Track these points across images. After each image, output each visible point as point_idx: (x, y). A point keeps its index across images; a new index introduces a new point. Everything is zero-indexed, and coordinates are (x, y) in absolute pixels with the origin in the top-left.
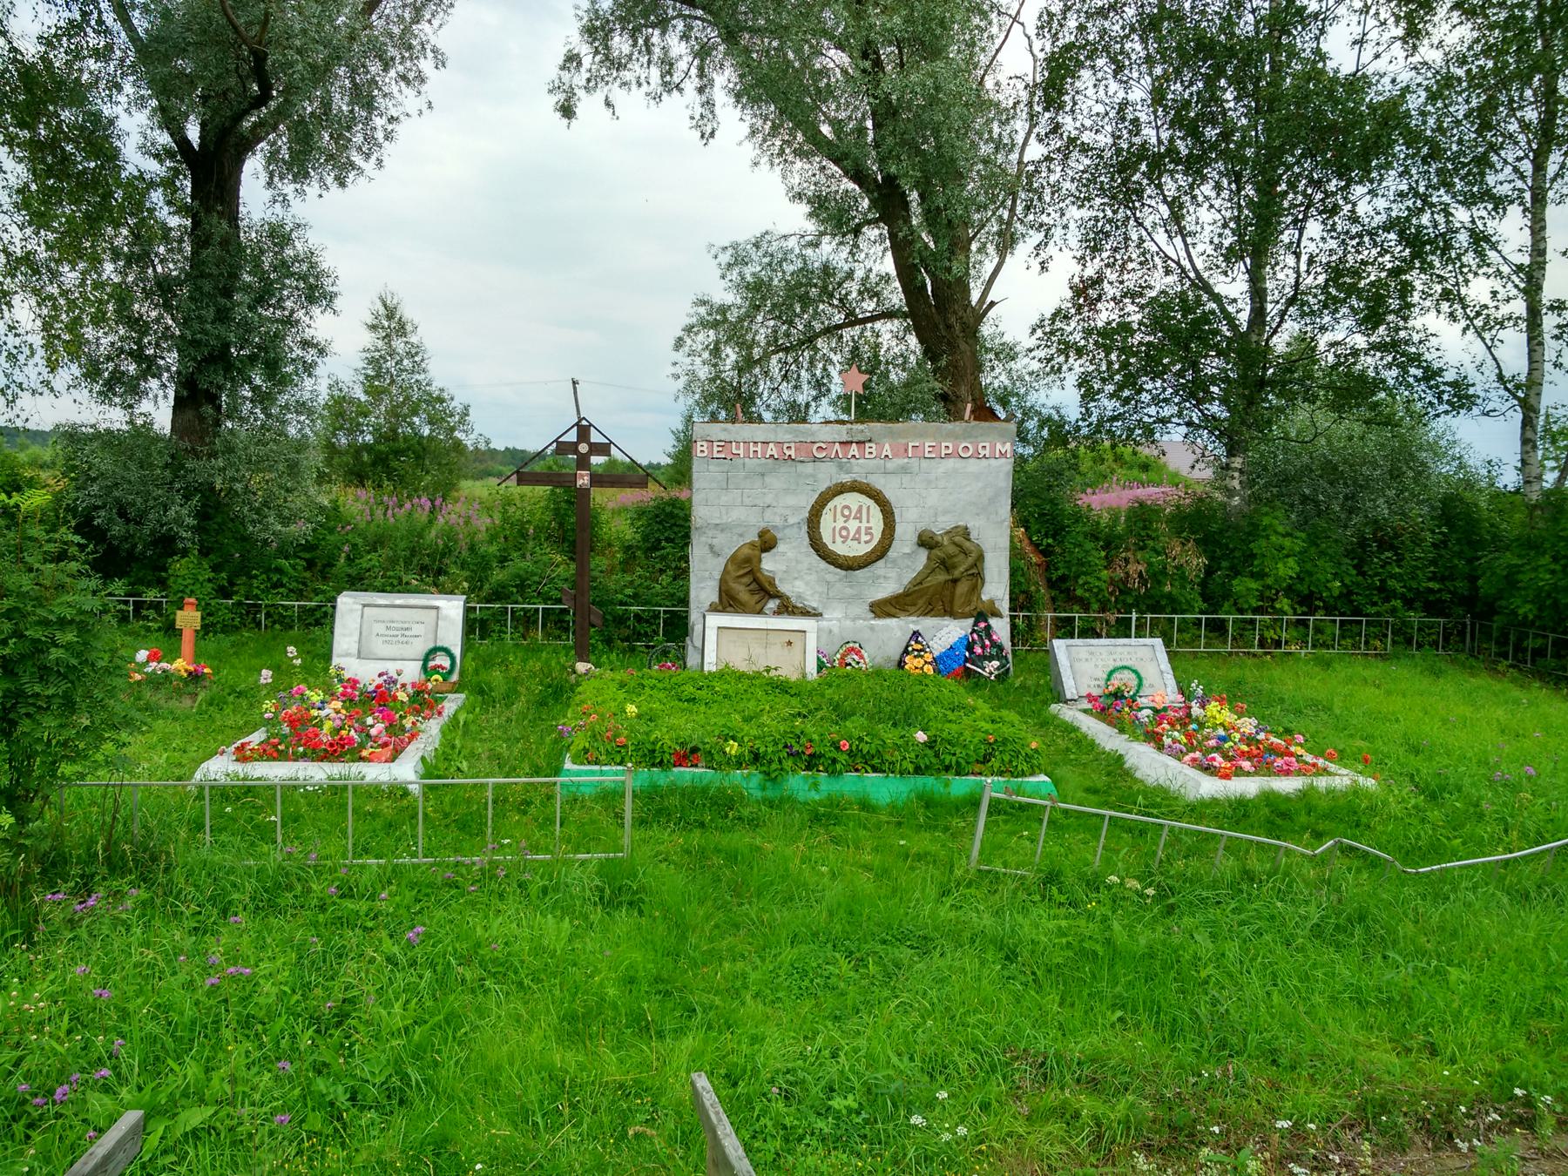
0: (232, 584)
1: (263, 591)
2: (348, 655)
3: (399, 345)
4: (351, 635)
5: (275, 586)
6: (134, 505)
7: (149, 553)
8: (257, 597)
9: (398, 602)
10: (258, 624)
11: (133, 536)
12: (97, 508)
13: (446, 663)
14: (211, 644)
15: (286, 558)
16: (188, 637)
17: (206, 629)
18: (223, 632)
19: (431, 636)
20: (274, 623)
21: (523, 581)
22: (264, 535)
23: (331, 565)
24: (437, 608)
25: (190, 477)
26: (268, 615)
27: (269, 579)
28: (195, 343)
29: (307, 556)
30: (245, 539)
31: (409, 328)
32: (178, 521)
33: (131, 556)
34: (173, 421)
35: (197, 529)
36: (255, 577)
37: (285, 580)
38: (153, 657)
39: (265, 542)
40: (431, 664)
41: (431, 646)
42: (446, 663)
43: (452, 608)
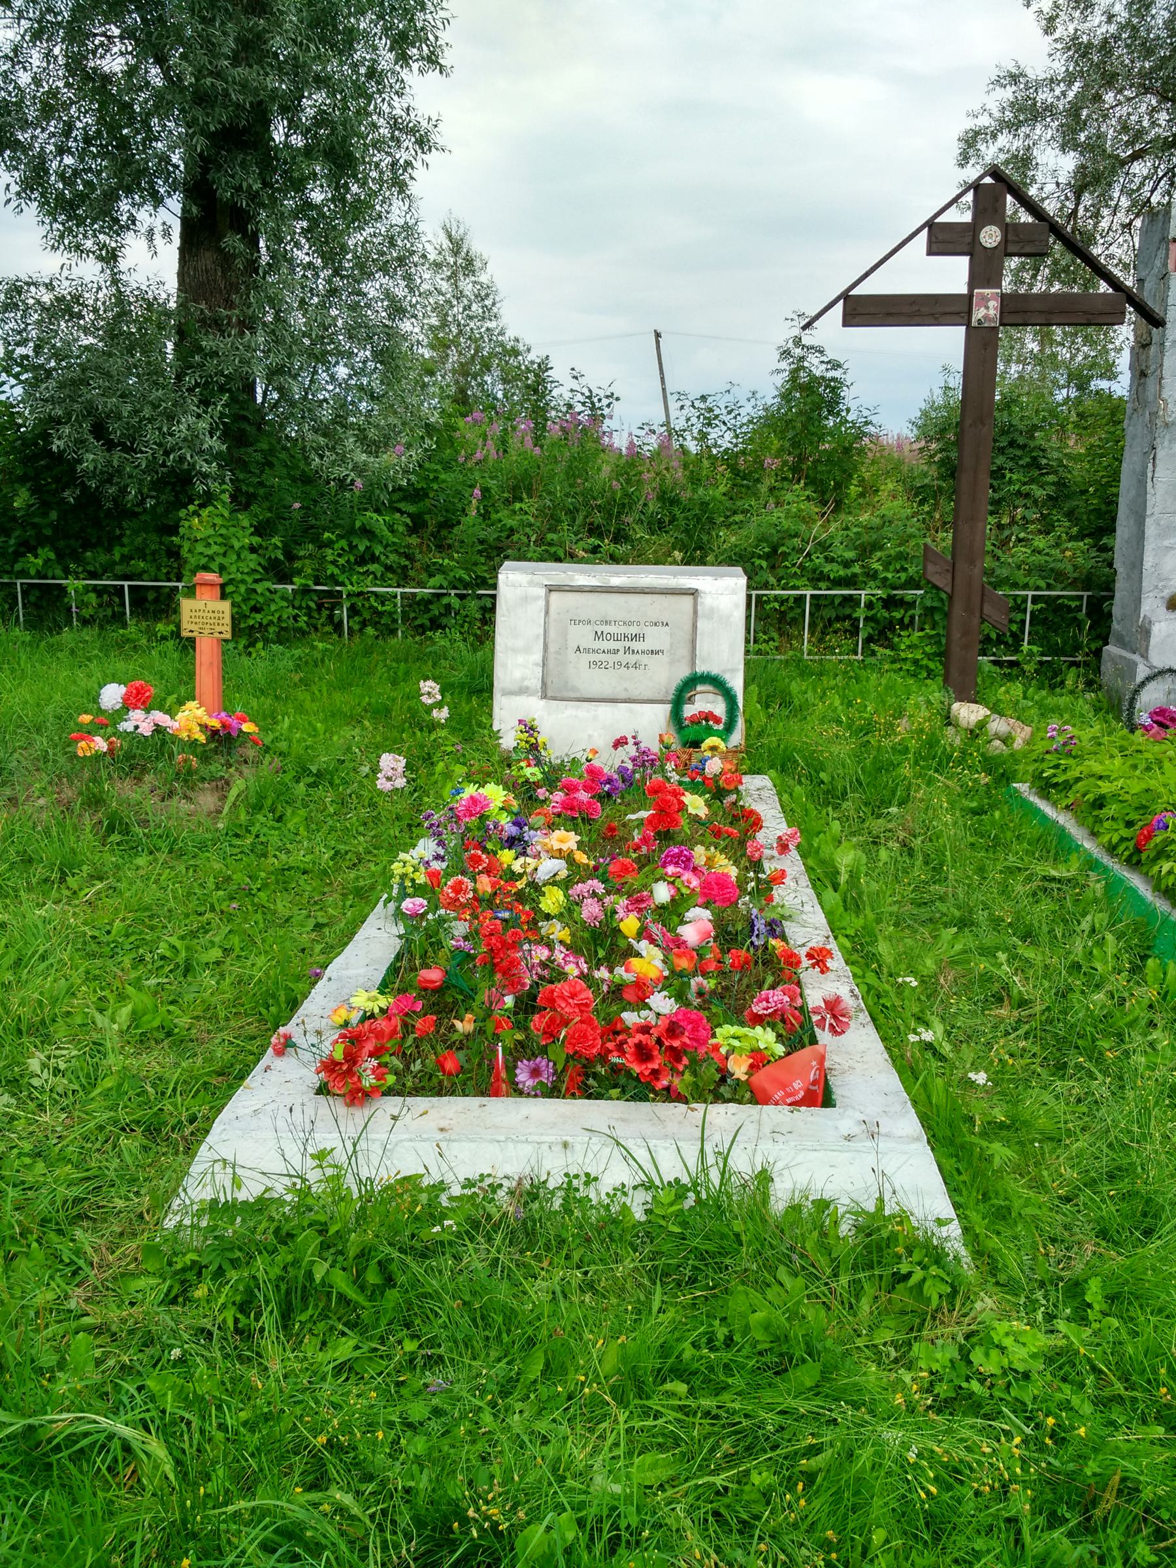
0: (291, 557)
1: (343, 569)
2: (522, 691)
3: (466, 285)
4: (527, 650)
5: (361, 561)
6: (119, 417)
7: (150, 502)
8: (334, 580)
9: (616, 581)
10: (338, 627)
11: (119, 471)
12: (58, 422)
13: (719, 708)
14: (261, 663)
15: (377, 511)
16: (206, 655)
17: (247, 631)
18: (280, 642)
19: (684, 652)
20: (364, 624)
21: (774, 550)
22: (340, 471)
23: (448, 525)
24: (694, 593)
25: (211, 365)
26: (353, 611)
27: (353, 548)
28: (202, 98)
29: (412, 509)
30: (307, 479)
31: (478, 264)
32: (192, 441)
33: (122, 512)
34: (181, 275)
35: (230, 461)
36: (330, 544)
37: (378, 549)
38: (136, 699)
39: (342, 483)
40: (689, 711)
41: (684, 672)
42: (719, 708)
43: (724, 592)
